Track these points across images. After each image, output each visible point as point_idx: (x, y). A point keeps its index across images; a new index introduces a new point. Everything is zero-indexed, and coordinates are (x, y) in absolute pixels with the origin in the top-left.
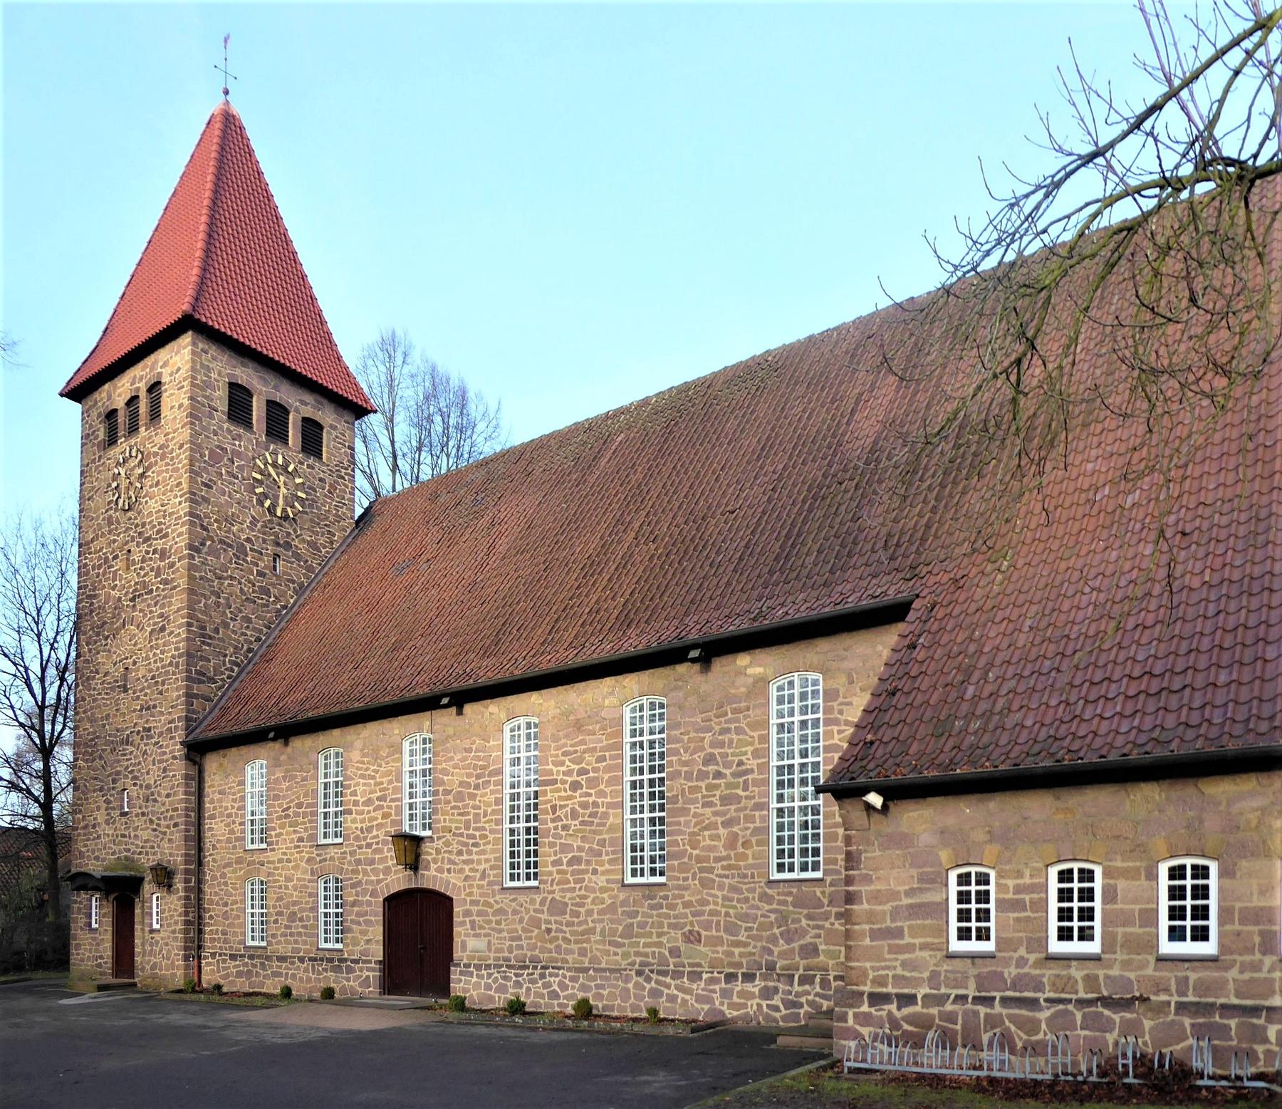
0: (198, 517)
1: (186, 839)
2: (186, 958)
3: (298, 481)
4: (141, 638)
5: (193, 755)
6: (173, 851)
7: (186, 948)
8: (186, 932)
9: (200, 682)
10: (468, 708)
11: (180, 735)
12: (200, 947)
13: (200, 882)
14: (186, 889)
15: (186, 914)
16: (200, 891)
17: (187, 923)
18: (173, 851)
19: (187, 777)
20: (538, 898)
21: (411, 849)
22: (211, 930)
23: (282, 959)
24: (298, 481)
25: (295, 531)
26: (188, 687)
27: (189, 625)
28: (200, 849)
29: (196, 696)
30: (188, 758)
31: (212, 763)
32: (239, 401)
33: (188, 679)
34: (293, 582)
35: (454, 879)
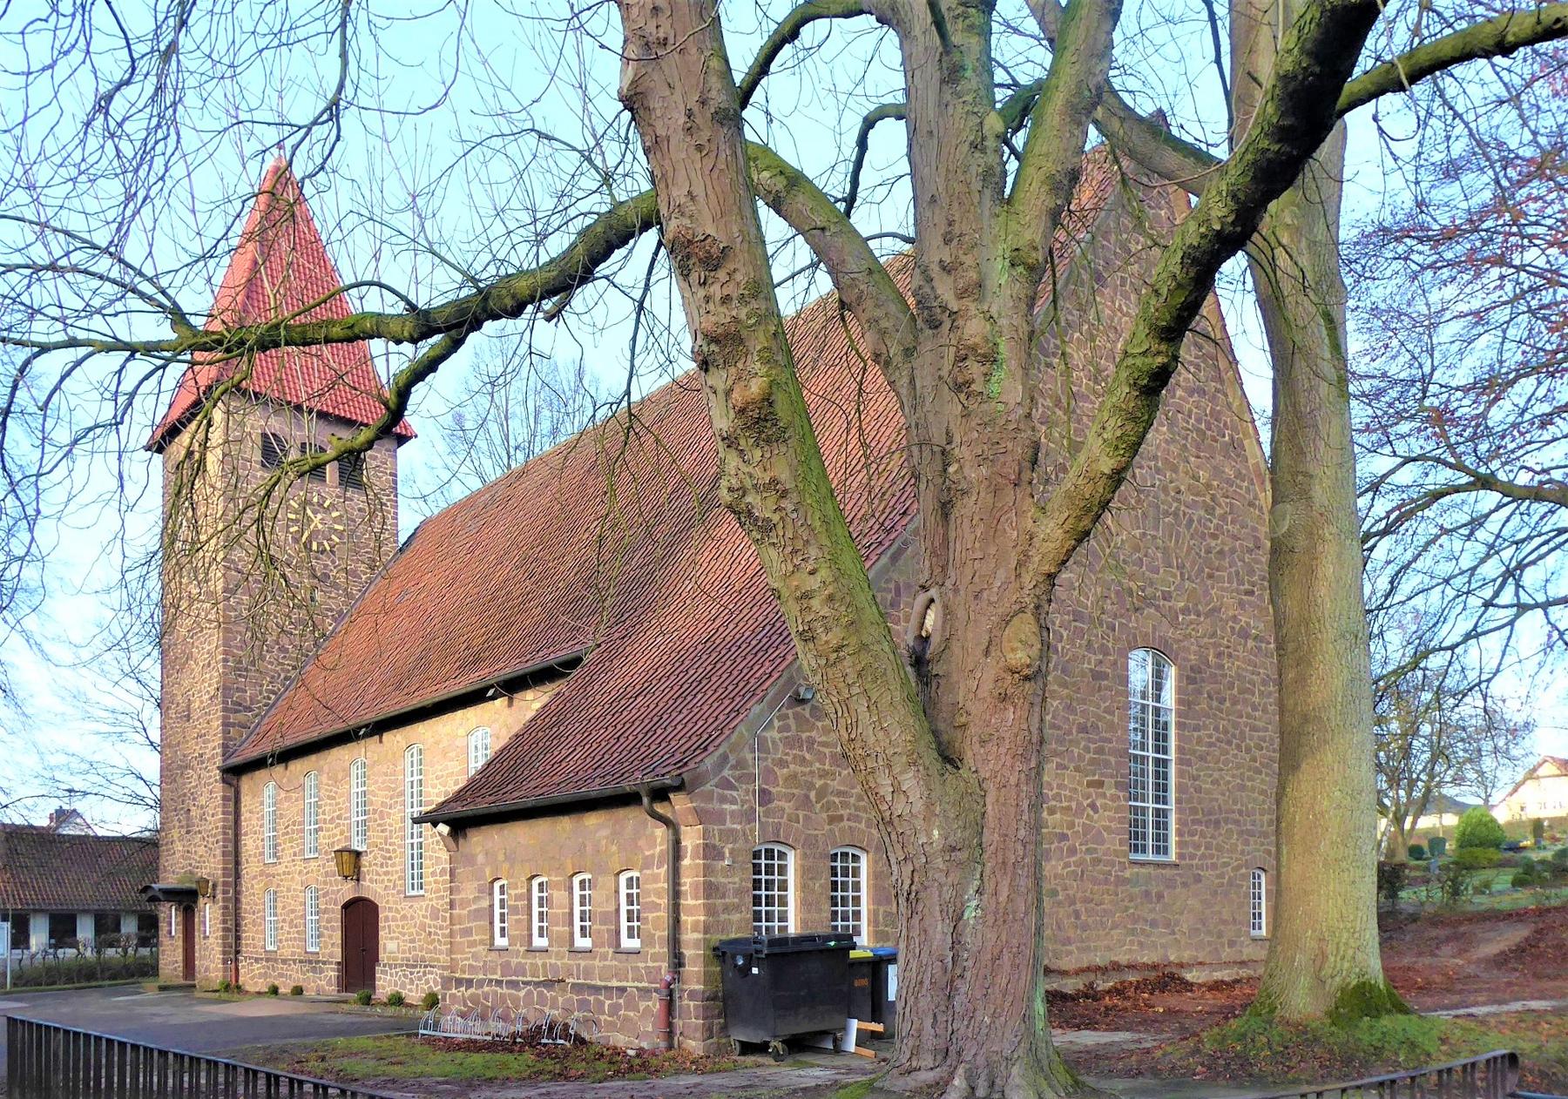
0: (233, 561)
1: (224, 854)
2: (225, 962)
3: (335, 514)
4: (198, 670)
5: (229, 776)
6: (211, 867)
7: (224, 953)
8: (224, 938)
9: (237, 711)
10: (387, 736)
11: (219, 761)
12: (238, 952)
13: (237, 893)
14: (224, 900)
15: (225, 922)
16: (237, 900)
17: (225, 930)
18: (211, 867)
19: (225, 798)
20: (424, 904)
21: (351, 863)
22: (248, 934)
23: (284, 961)
24: (335, 514)
25: (333, 562)
26: (224, 717)
27: (225, 660)
28: (237, 863)
29: (233, 725)
30: (224, 781)
31: (246, 783)
32: (270, 451)
33: (225, 710)
34: (331, 610)
35: (379, 888)
